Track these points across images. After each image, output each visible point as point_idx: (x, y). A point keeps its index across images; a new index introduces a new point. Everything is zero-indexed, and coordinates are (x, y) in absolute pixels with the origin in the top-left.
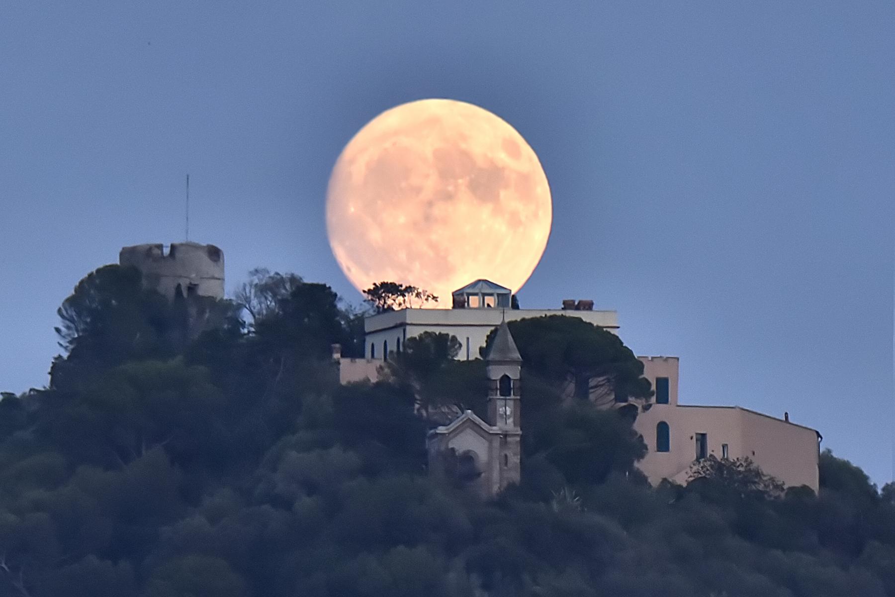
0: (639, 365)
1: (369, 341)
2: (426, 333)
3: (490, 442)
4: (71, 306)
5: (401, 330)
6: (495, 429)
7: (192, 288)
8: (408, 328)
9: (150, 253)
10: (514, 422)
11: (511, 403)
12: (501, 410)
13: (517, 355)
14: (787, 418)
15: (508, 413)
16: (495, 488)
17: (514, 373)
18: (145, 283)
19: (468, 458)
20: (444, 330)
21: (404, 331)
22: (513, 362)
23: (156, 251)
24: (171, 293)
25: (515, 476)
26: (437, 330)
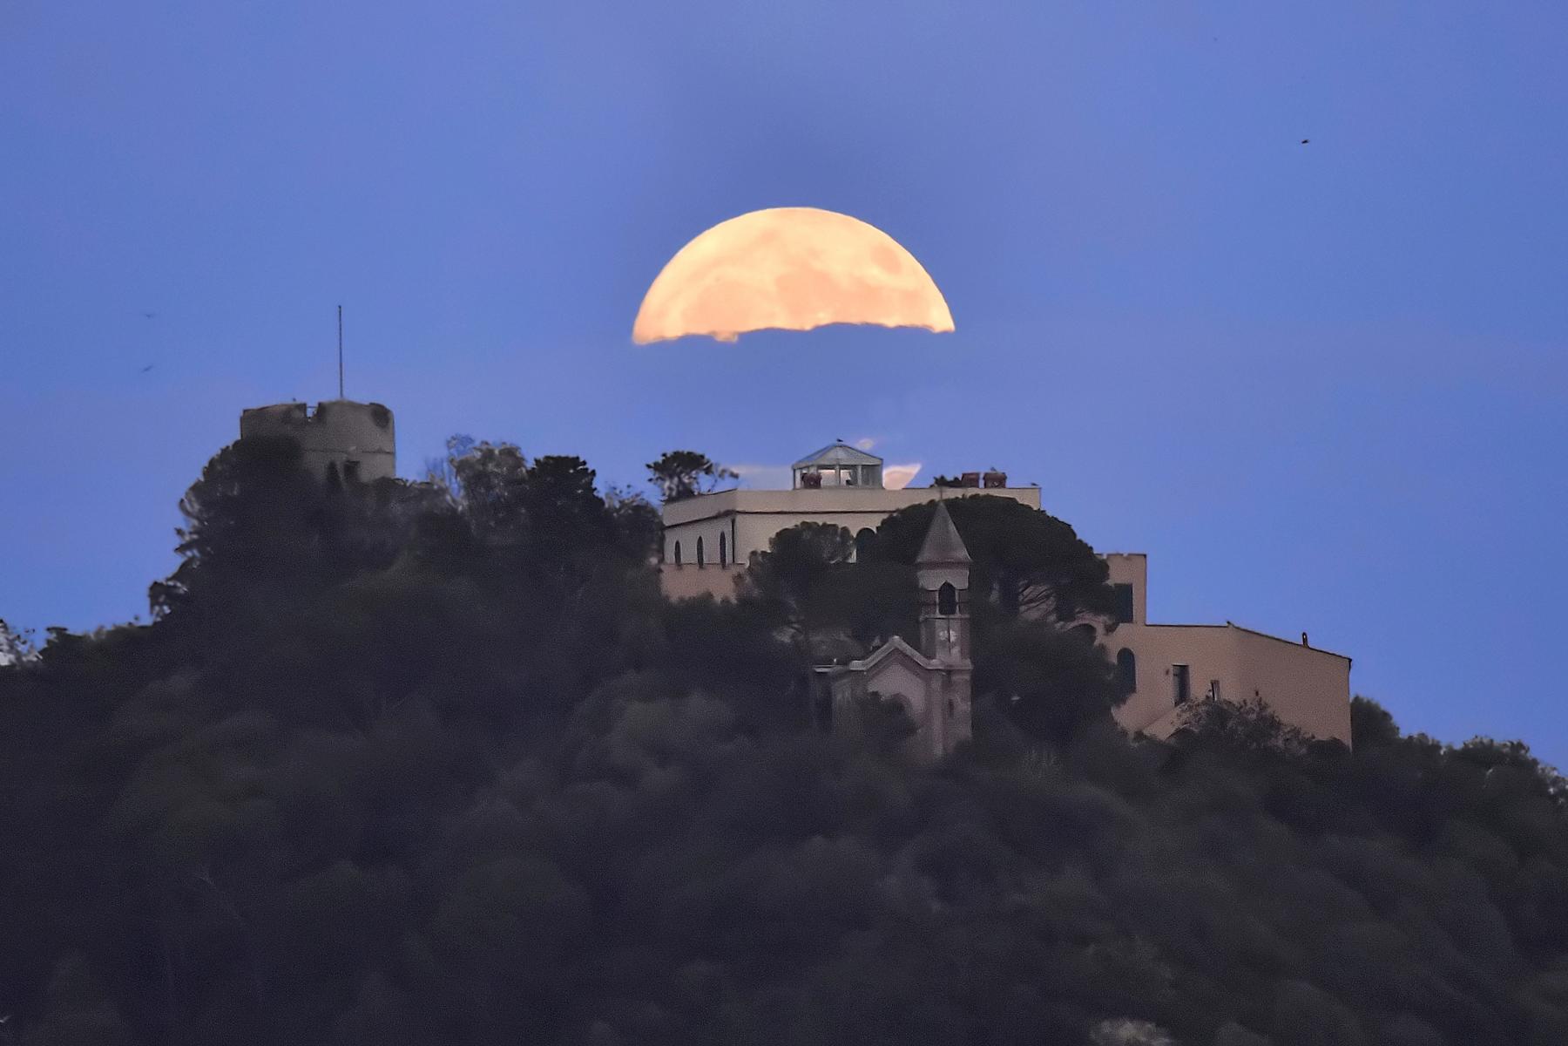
0: (1102, 567)
1: (670, 540)
2: (804, 523)
3: (928, 682)
4: (198, 497)
5: (728, 520)
6: (935, 663)
7: (351, 468)
8: (739, 518)
9: (291, 414)
10: (962, 652)
11: (956, 625)
12: (942, 635)
13: (962, 554)
14: (1305, 640)
15: (953, 639)
16: (938, 751)
17: (960, 580)
18: (316, 463)
19: (897, 706)
20: (830, 520)
21: (733, 522)
22: (959, 564)
23: (297, 414)
24: (321, 474)
25: (964, 731)
26: (820, 520)
